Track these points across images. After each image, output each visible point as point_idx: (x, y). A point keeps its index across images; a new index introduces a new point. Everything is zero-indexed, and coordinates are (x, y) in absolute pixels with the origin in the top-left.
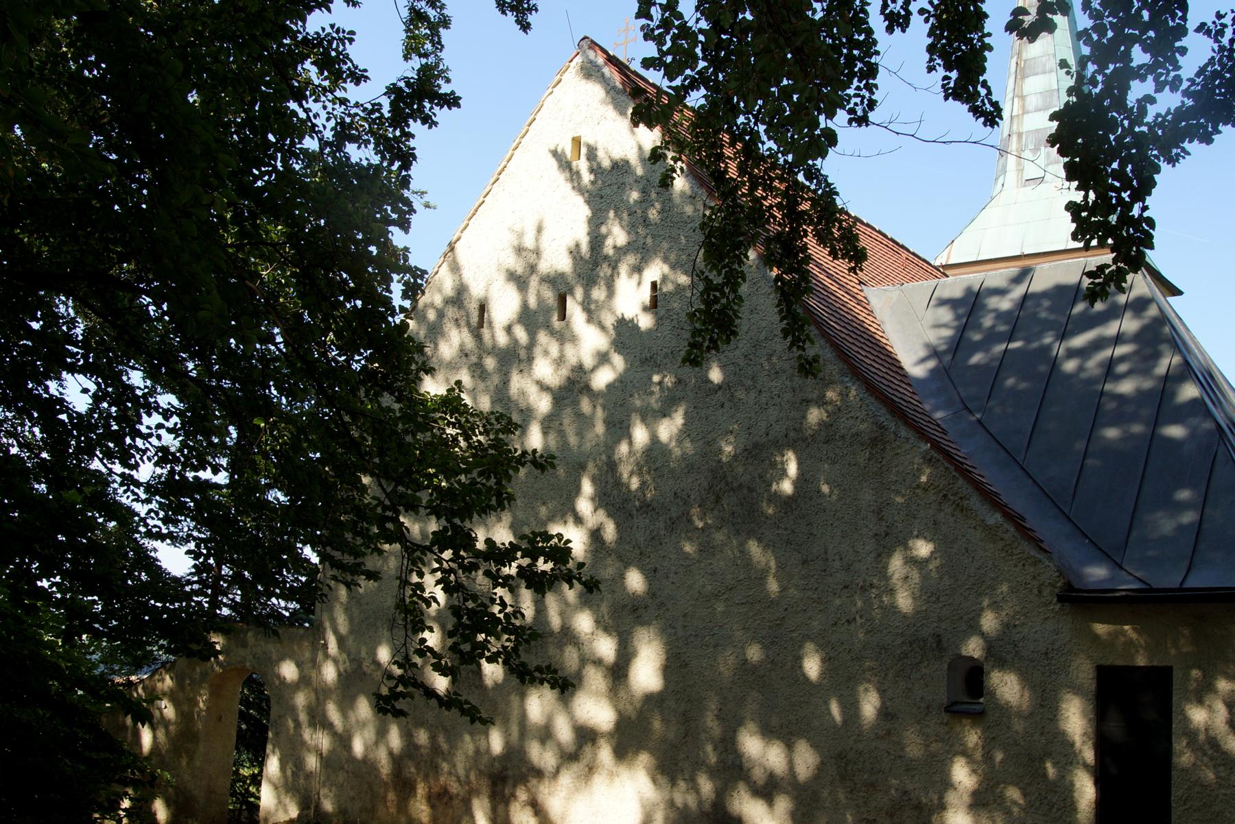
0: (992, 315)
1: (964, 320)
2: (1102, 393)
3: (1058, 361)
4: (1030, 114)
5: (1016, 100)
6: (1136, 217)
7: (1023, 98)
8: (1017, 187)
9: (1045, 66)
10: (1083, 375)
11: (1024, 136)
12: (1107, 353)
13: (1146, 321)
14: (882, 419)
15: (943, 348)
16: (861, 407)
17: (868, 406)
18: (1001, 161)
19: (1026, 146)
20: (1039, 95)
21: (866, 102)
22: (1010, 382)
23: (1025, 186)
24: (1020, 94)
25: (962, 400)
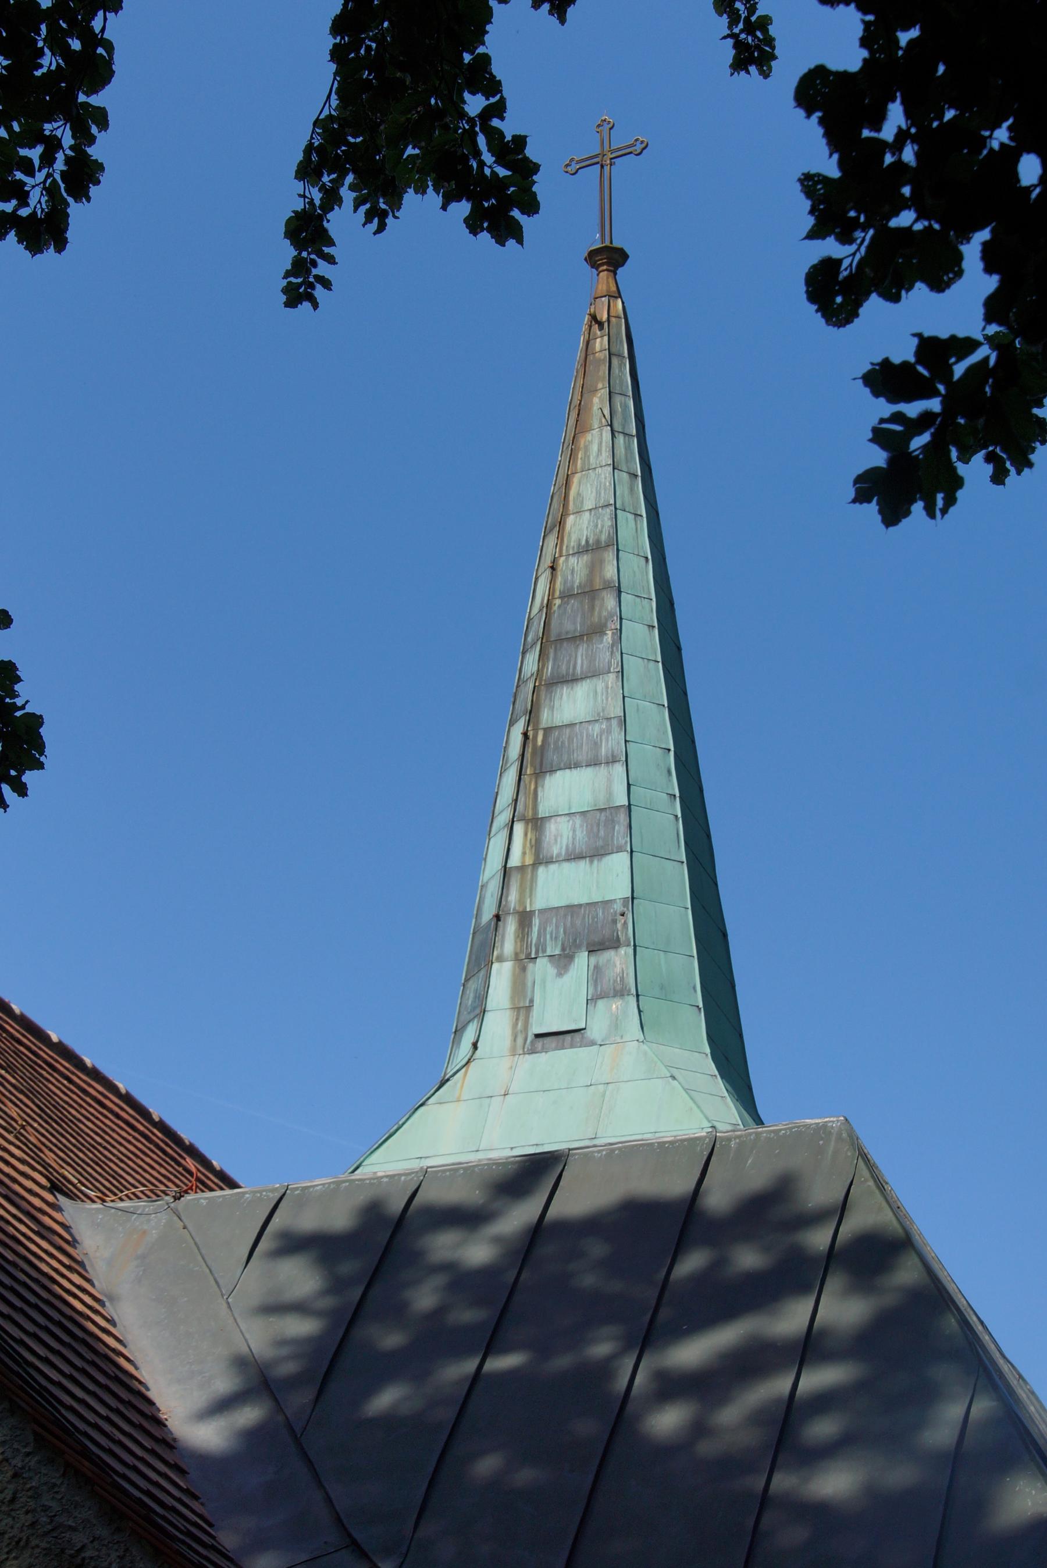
0: (439, 1280)
1: (356, 1293)
2: (765, 1499)
3: (630, 1408)
4: (553, 867)
5: (519, 828)
6: (1036, 411)
7: (536, 823)
8: (513, 1052)
9: (596, 745)
10: (706, 1448)
11: (536, 922)
12: (780, 1385)
13: (888, 1300)
14: (79, 1539)
15: (289, 1368)
16: (13, 1500)
17: (36, 1496)
18: (472, 985)
19: (541, 947)
20: (578, 820)
21: (60, 165)
22: (487, 1466)
23: (533, 1051)
24: (530, 814)
25: (339, 1520)
